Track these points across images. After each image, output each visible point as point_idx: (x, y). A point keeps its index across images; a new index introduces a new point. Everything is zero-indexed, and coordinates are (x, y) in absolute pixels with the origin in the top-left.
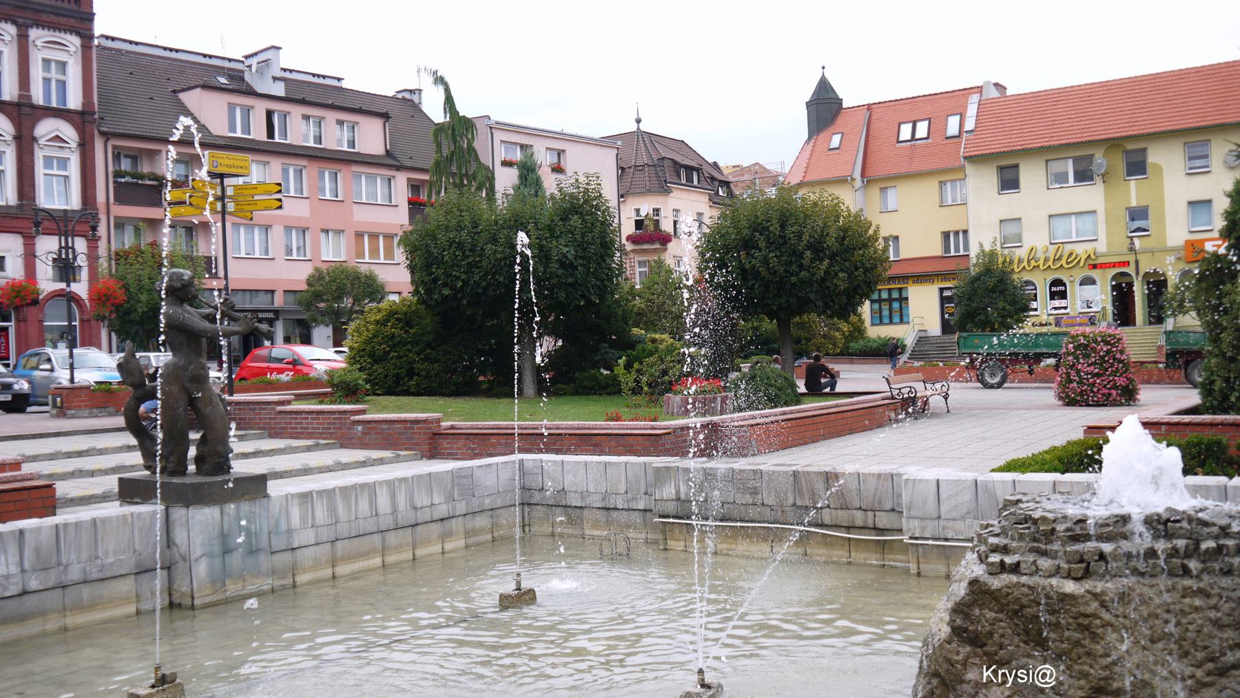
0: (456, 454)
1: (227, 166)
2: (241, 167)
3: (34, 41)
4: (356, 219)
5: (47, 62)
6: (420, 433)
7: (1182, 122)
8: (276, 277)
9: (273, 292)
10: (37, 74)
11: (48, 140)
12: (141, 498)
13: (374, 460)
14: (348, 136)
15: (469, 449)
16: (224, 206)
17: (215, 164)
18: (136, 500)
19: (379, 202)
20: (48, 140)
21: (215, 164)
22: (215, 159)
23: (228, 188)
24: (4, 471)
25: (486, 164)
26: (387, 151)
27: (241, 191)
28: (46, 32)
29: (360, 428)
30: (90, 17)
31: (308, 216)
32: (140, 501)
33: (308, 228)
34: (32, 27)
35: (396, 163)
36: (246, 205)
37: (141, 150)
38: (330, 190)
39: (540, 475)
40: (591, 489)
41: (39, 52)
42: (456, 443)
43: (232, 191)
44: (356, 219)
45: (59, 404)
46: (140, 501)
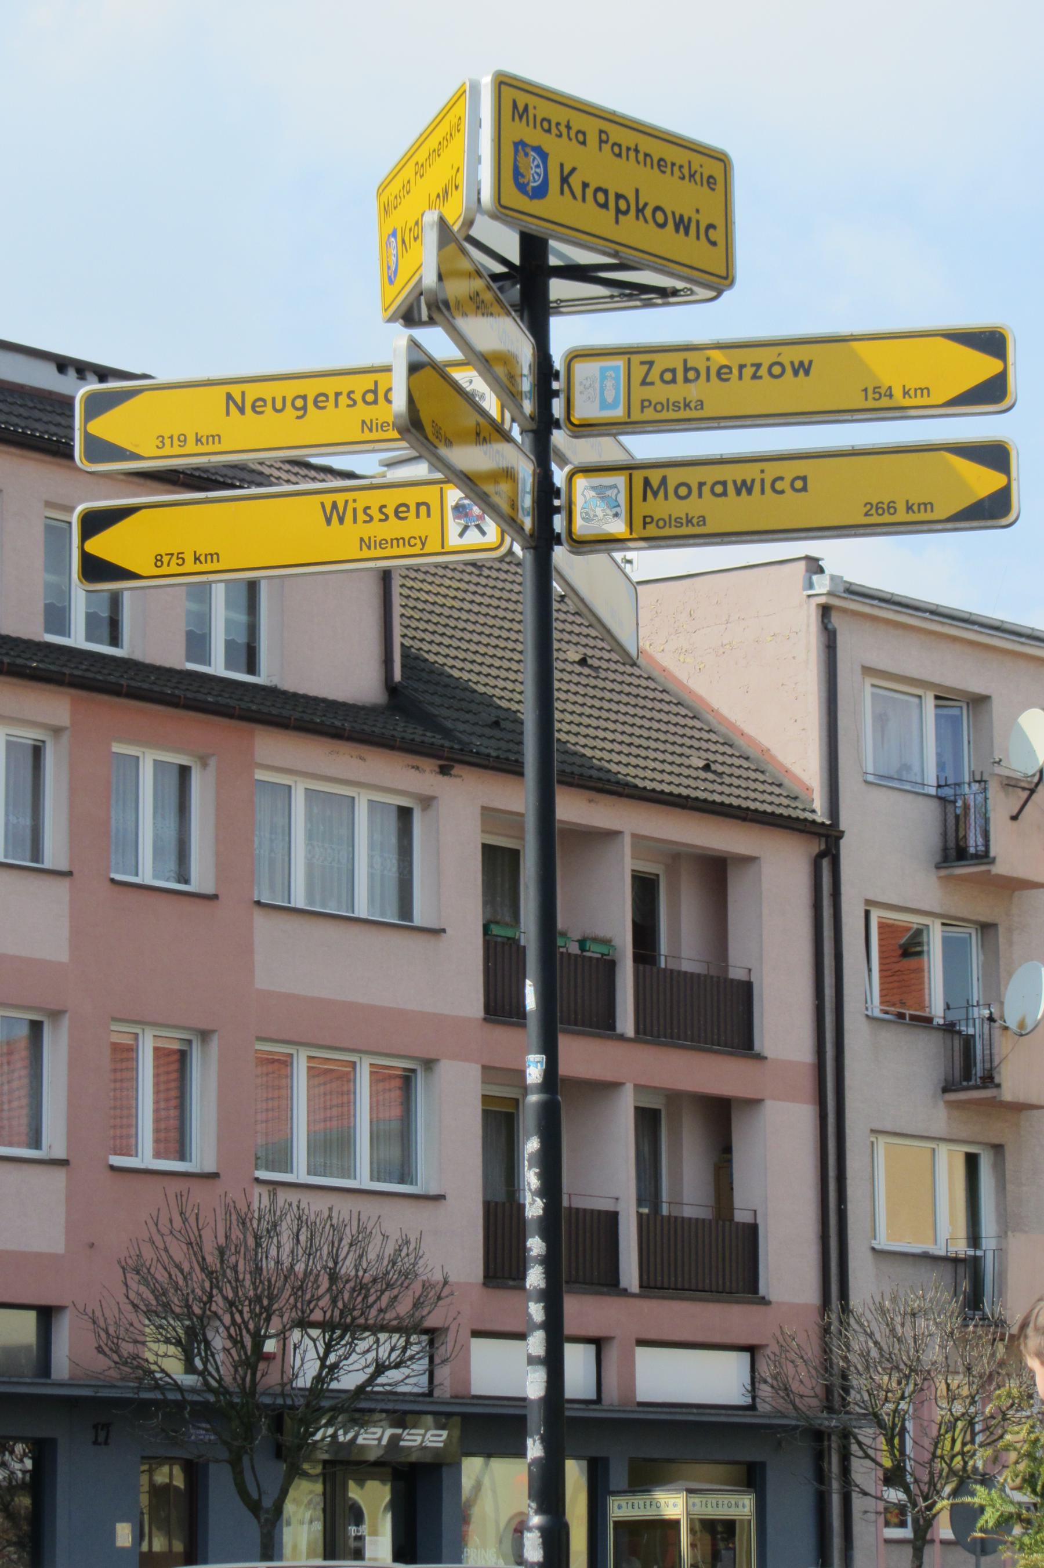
1: (602, 197)
2: (682, 224)
4: (263, 981)
7: (659, 1260)
14: (228, 622)
19: (362, 910)
21: (533, 175)
22: (534, 137)
23: (583, 370)
26: (392, 689)
27: (678, 392)
31: (63, 955)
35: (438, 740)
38: (158, 851)
44: (263, 981)
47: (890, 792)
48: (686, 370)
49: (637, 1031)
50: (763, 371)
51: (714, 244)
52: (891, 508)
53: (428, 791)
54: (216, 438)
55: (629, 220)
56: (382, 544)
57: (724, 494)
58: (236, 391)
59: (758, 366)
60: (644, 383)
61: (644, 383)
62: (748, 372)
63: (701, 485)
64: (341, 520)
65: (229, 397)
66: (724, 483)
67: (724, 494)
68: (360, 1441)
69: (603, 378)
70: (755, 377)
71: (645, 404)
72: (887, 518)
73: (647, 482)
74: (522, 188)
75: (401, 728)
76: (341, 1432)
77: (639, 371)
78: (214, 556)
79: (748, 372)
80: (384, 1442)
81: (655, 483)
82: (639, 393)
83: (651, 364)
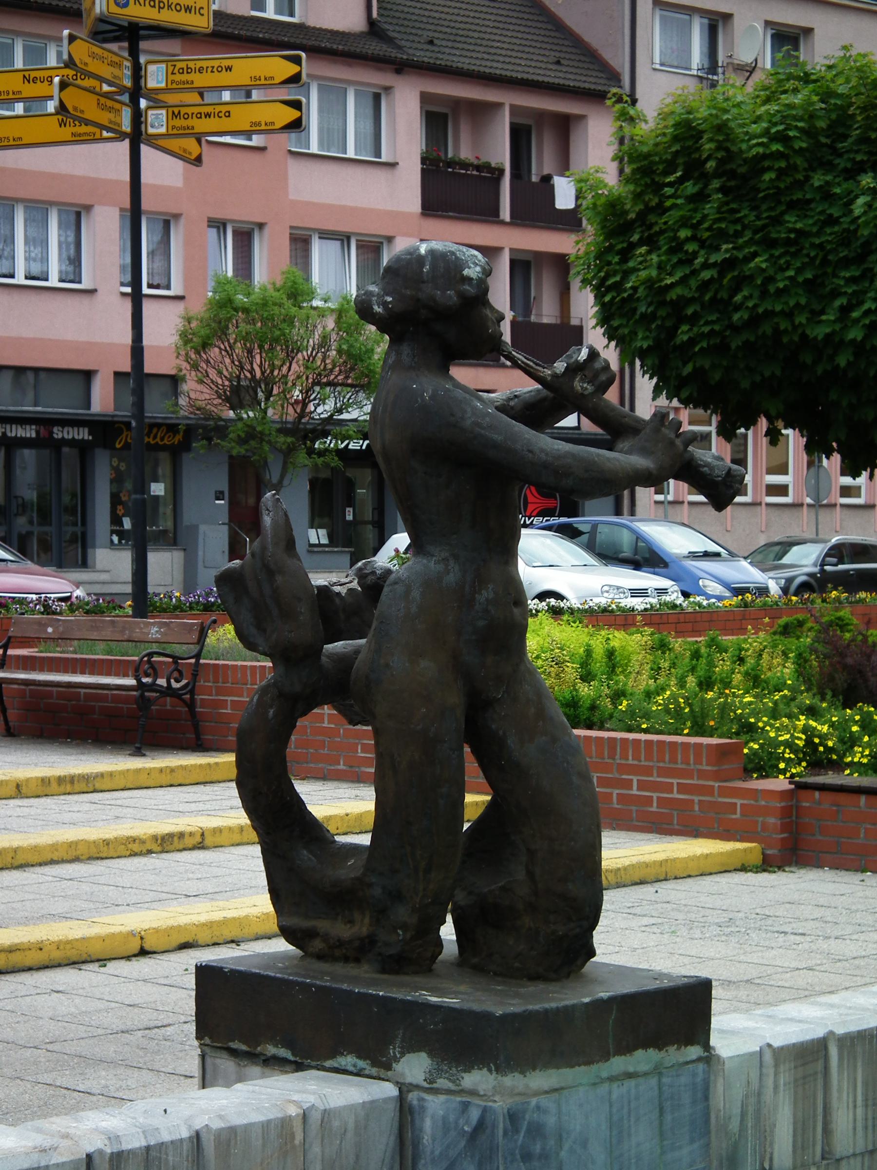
4: (292, 196)
8: (98, 339)
9: (88, 375)
12: (289, 1044)
16: (138, 117)
18: (271, 1050)
19: (351, 154)
25: (614, 63)
26: (371, 23)
27: (185, 77)
32: (284, 1053)
33: (177, 216)
36: (199, 116)
43: (162, 76)
44: (292, 196)
46: (284, 1053)
47: (668, 74)
48: (188, 68)
49: (512, 217)
50: (215, 70)
51: (202, 15)
52: (259, 124)
53: (388, 84)
54: (20, 92)
55: (165, 11)
56: (80, 135)
57: (201, 117)
58: (26, 73)
59: (213, 67)
60: (172, 73)
61: (172, 73)
62: (210, 70)
63: (193, 114)
64: (65, 126)
65: (24, 76)
66: (201, 113)
67: (201, 117)
68: (350, 447)
69: (158, 71)
70: (212, 72)
71: (173, 82)
72: (258, 128)
73: (173, 113)
74: (117, 4)
75: (375, 47)
76: (340, 442)
77: (170, 69)
78: (20, 139)
79: (210, 70)
80: (364, 447)
81: (176, 113)
82: (171, 77)
83: (175, 66)
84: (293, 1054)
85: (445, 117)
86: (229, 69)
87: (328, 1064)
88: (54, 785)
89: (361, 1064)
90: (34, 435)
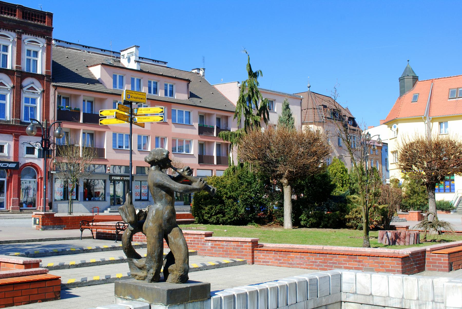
0: (268, 262)
2: (142, 99)
3: (24, 41)
5: (29, 52)
6: (246, 249)
10: (24, 56)
11: (27, 89)
12: (131, 296)
13: (223, 264)
15: (276, 259)
17: (129, 97)
18: (127, 297)
19: (184, 123)
20: (27, 89)
21: (129, 97)
24: (6, 252)
28: (30, 36)
29: (210, 244)
30: (50, 29)
32: (130, 298)
34: (23, 34)
36: (143, 119)
37: (71, 95)
39: (354, 284)
40: (392, 295)
41: (26, 46)
42: (268, 256)
45: (37, 223)
84: (132, 298)
85: (203, 116)
86: (149, 110)
87: (137, 300)
88: (110, 249)
89: (143, 300)
90: (120, 179)
